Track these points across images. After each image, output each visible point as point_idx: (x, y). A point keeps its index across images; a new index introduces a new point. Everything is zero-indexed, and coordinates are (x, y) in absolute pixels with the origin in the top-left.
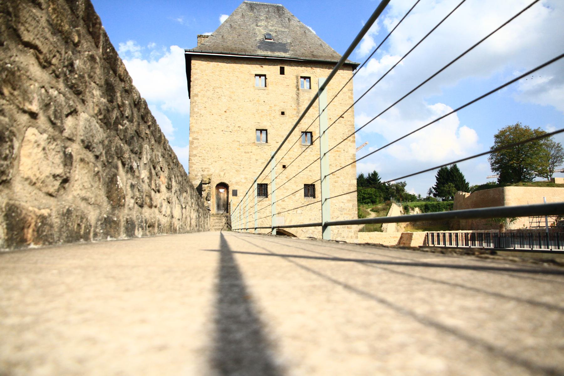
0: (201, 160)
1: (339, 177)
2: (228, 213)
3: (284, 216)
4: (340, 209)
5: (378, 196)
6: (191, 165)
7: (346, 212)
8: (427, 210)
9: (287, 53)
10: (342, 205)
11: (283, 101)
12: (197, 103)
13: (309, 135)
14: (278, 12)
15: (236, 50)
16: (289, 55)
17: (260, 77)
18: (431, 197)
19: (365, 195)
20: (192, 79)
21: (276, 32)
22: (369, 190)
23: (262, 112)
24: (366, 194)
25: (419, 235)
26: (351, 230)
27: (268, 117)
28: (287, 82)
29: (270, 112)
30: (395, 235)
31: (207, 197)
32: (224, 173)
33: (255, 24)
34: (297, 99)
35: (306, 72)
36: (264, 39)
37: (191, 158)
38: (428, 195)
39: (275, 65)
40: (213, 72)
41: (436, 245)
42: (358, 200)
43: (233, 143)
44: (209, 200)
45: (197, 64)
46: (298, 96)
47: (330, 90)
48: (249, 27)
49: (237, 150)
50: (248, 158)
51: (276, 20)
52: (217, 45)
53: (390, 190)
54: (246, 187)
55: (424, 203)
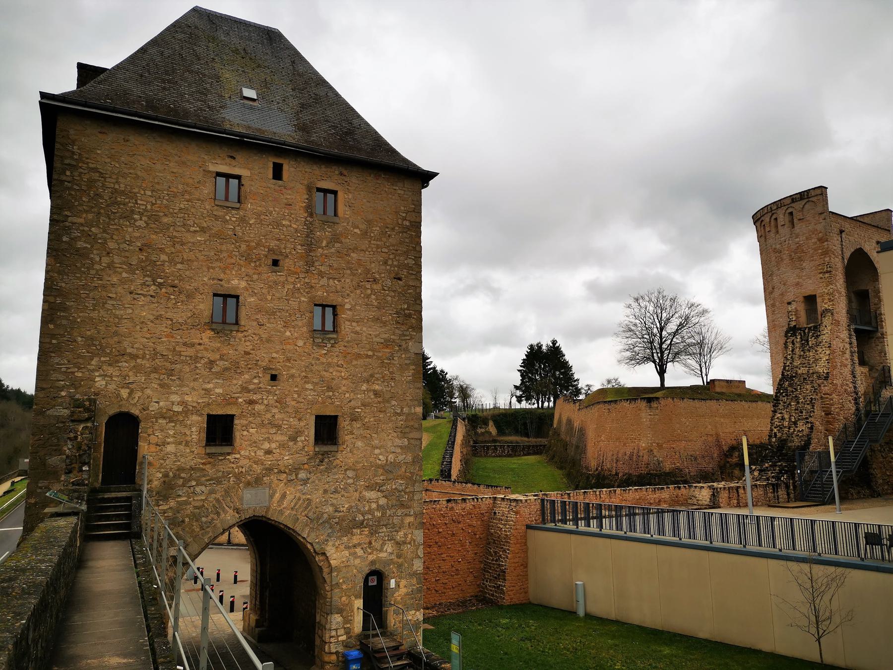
13: (329, 311)
14: (271, 44)
27: (243, 269)
43: (157, 322)
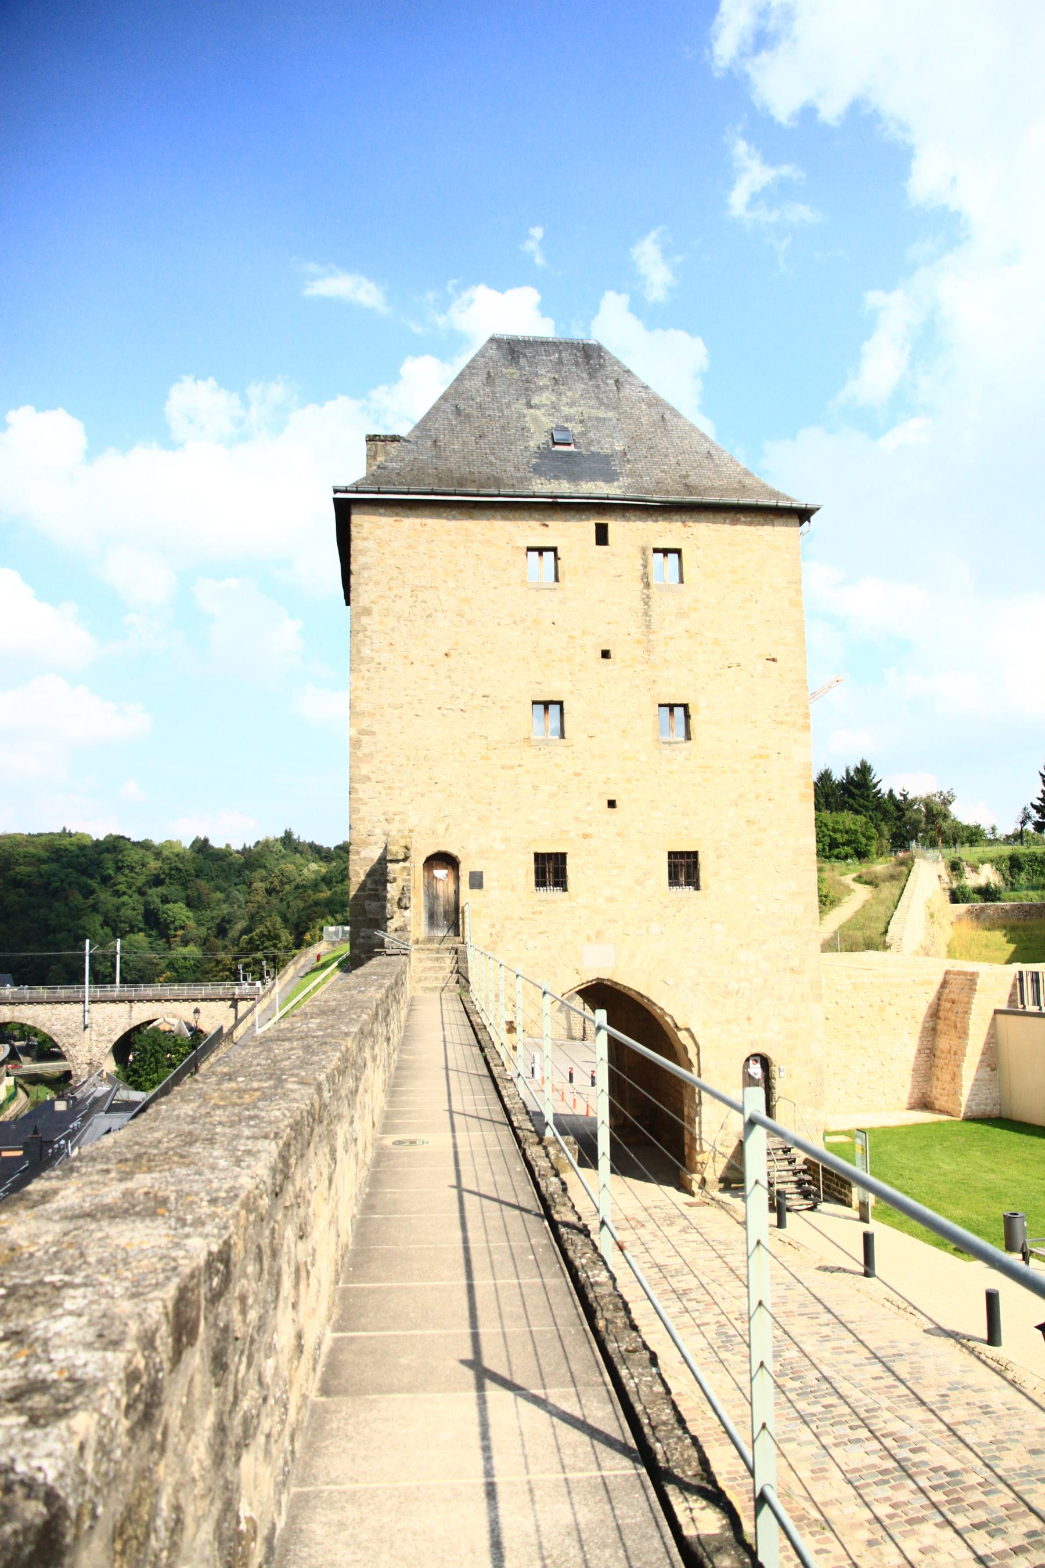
0: (383, 792)
1: (765, 830)
2: (458, 935)
5: (873, 838)
6: (355, 805)
8: (1016, 870)
9: (616, 483)
12: (368, 633)
13: (679, 712)
14: (588, 363)
15: (474, 481)
16: (620, 488)
19: (838, 836)
20: (353, 567)
21: (581, 422)
22: (848, 819)
23: (549, 651)
24: (841, 831)
31: (400, 899)
32: (444, 826)
33: (524, 401)
34: (646, 614)
36: (551, 443)
37: (356, 785)
39: (581, 520)
40: (410, 547)
44: (406, 908)
45: (366, 525)
46: (646, 603)
48: (506, 412)
51: (582, 386)
52: (422, 468)
53: (908, 814)
55: (1007, 850)
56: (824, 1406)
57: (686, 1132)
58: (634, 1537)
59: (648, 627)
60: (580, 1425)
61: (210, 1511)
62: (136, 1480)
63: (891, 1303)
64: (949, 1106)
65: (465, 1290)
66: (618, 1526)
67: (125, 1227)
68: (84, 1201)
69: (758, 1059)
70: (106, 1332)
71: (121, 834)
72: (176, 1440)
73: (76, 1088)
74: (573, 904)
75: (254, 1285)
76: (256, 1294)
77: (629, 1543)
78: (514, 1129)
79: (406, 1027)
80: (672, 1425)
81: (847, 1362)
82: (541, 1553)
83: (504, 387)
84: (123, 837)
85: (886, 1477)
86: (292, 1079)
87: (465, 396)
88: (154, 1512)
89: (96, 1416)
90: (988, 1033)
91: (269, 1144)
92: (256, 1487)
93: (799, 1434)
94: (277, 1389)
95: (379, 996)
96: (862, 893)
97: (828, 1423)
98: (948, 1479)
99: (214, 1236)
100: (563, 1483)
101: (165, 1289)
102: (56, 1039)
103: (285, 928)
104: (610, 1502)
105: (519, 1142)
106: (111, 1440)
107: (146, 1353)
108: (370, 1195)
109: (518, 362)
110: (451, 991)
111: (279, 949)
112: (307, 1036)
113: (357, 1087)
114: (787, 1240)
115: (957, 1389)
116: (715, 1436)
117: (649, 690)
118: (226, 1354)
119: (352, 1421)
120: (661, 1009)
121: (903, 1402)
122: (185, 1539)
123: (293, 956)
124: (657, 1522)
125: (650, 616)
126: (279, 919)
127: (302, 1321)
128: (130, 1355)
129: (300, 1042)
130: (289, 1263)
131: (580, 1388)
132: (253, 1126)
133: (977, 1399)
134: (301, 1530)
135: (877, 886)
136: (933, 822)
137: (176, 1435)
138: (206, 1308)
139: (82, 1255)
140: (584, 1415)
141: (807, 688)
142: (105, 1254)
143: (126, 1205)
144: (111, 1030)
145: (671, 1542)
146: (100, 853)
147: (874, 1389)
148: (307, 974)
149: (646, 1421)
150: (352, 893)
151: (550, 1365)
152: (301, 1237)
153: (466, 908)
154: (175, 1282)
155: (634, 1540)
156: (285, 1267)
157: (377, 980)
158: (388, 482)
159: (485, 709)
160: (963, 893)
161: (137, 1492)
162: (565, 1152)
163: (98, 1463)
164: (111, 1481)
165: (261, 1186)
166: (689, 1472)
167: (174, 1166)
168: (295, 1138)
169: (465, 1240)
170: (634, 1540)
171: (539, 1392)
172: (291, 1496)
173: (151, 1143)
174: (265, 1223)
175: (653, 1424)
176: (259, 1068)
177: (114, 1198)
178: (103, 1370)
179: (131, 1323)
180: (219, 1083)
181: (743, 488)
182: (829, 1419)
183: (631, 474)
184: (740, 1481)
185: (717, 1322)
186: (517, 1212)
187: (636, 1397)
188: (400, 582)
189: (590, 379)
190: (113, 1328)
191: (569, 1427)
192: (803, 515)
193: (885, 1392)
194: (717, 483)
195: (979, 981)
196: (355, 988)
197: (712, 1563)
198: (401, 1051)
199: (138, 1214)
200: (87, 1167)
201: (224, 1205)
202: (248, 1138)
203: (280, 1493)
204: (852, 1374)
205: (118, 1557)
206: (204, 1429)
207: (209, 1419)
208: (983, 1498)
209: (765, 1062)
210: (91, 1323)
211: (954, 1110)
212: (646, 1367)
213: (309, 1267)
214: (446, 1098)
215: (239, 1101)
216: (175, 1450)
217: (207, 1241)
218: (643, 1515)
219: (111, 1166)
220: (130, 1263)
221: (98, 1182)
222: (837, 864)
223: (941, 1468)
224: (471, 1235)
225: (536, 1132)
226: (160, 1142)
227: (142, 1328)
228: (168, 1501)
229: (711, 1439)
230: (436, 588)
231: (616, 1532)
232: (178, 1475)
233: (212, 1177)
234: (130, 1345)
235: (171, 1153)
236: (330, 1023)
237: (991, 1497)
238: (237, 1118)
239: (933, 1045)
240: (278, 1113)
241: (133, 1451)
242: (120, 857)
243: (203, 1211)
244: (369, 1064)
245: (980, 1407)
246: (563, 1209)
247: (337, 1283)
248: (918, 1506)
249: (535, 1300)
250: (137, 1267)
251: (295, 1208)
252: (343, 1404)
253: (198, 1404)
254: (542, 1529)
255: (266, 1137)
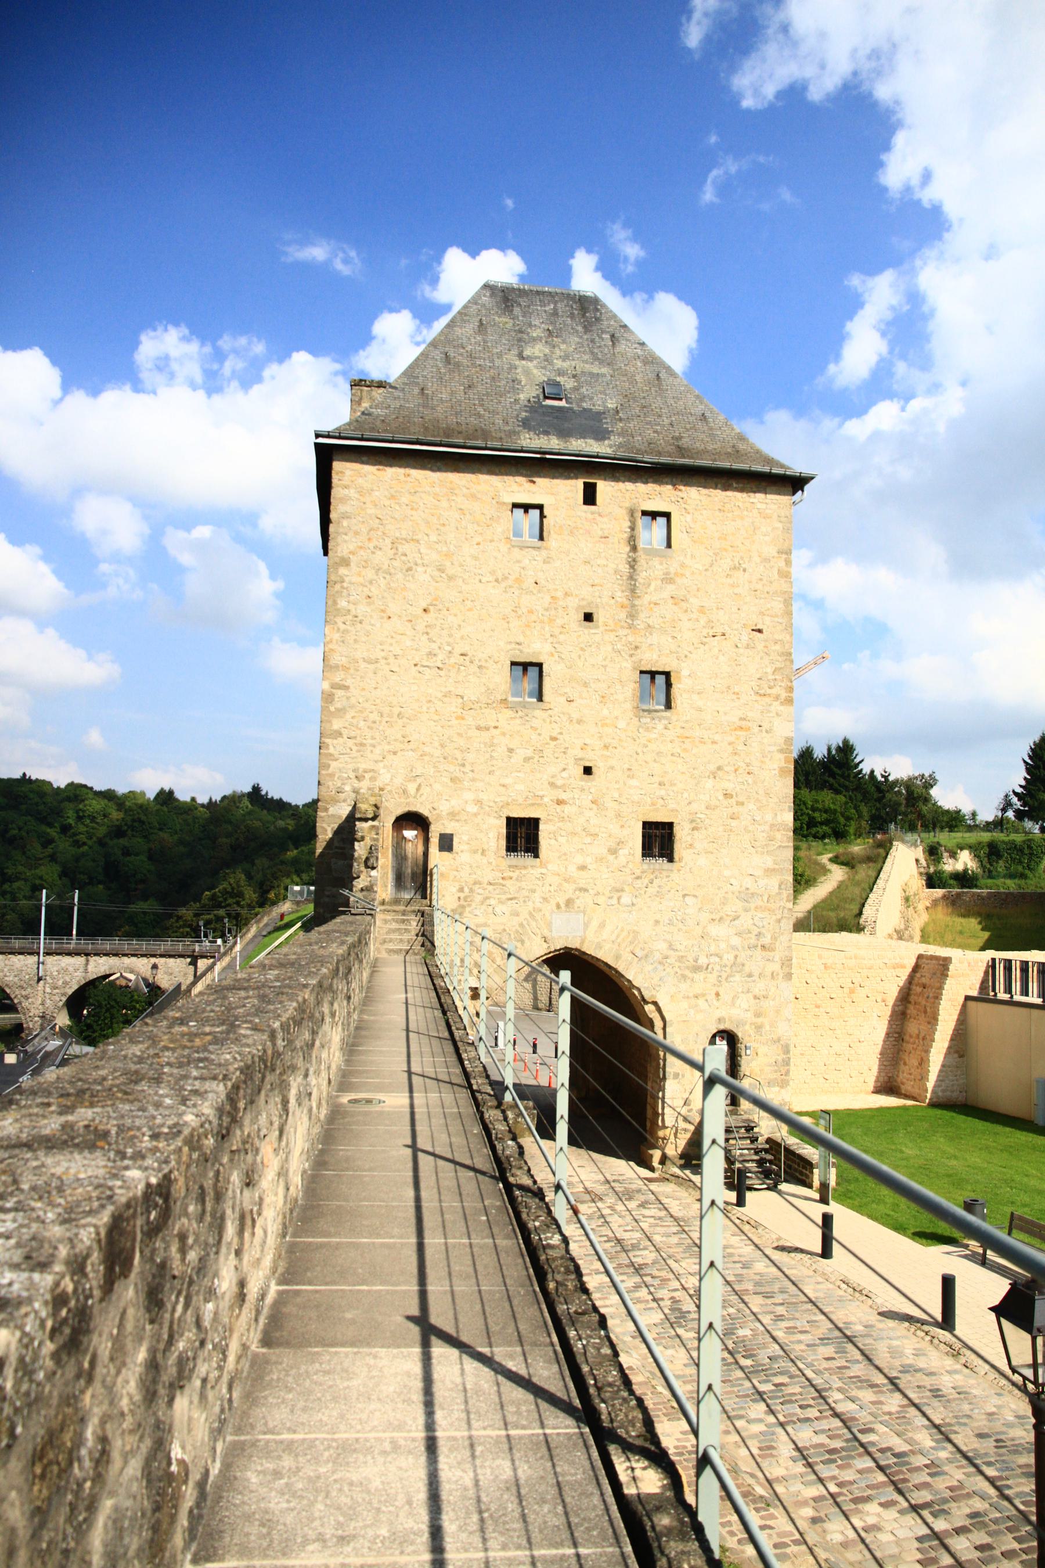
0: (355, 748)
1: (742, 804)
3: (584, 912)
4: (743, 895)
5: (852, 819)
6: (324, 761)
7: (760, 903)
8: (994, 858)
9: (606, 442)
10: (748, 882)
11: (591, 582)
12: (345, 585)
13: (660, 680)
14: (584, 316)
15: (460, 433)
16: (610, 446)
17: (526, 512)
18: (1008, 820)
19: (817, 815)
20: (333, 515)
21: (574, 376)
22: (827, 798)
23: (531, 612)
24: (820, 810)
25: (969, 964)
26: (771, 954)
27: (547, 628)
28: (604, 526)
29: (553, 612)
30: (898, 961)
31: (367, 859)
32: (415, 786)
33: (515, 352)
34: (631, 577)
35: (658, 498)
36: (541, 397)
37: (327, 741)
38: (1000, 814)
40: (393, 497)
41: (1018, 998)
42: (795, 831)
43: (446, 700)
44: (373, 868)
45: (348, 473)
46: (632, 567)
47: (726, 550)
48: (498, 362)
49: (454, 722)
50: (485, 744)
51: (577, 339)
53: (888, 796)
54: (478, 824)
55: (986, 837)
56: (775, 1385)
57: (648, 1107)
58: (574, 1494)
59: (633, 591)
60: (525, 1383)
61: (138, 1447)
62: (59, 1406)
63: (847, 1284)
64: (915, 1091)
65: (414, 1248)
66: (558, 1484)
67: (62, 1158)
68: (21, 1131)
69: (725, 1035)
70: (34, 1255)
71: (84, 782)
72: (105, 1371)
73: (28, 1042)
74: (544, 871)
75: (195, 1225)
76: (197, 1235)
77: (568, 1500)
78: (473, 1092)
79: (368, 988)
80: (618, 1387)
81: (800, 1342)
82: (479, 1506)
83: (495, 337)
84: (85, 786)
85: (833, 1457)
86: (245, 1026)
87: (455, 343)
88: (79, 1440)
89: (18, 1334)
90: (958, 1020)
91: (218, 1085)
92: (189, 1431)
93: (748, 1411)
94: (216, 1335)
95: (340, 952)
96: (837, 874)
97: (778, 1401)
98: (895, 1460)
99: (154, 1169)
100: (505, 1440)
101: (100, 1216)
102: (8, 991)
103: (249, 886)
104: (552, 1460)
105: (477, 1104)
106: (34, 1360)
107: (76, 1278)
108: (322, 1152)
109: (512, 311)
110: (416, 954)
111: (243, 907)
112: (263, 986)
113: (314, 1041)
114: (745, 1219)
115: (908, 1372)
116: (664, 1411)
117: (631, 656)
118: (162, 1291)
119: (293, 1372)
120: (629, 981)
121: (854, 1383)
122: (111, 1473)
123: (256, 915)
124: (597, 1480)
125: (636, 580)
126: (243, 876)
127: (245, 1270)
128: (58, 1277)
129: (256, 992)
130: (233, 1208)
131: (527, 1348)
132: (202, 1068)
133: (927, 1382)
134: (235, 1478)
135: (853, 867)
136: (913, 806)
137: (105, 1367)
138: (142, 1241)
139: (15, 1182)
140: (529, 1374)
141: (792, 662)
142: (39, 1182)
143: (65, 1137)
144: (66, 983)
145: (611, 1500)
146: (62, 801)
147: (826, 1369)
148: (270, 933)
149: (592, 1382)
150: (319, 851)
151: (497, 1324)
152: (248, 1185)
153: (435, 870)
154: (110, 1208)
155: (573, 1497)
156: (229, 1212)
157: (338, 937)
158: (372, 429)
159: (462, 668)
160: (940, 879)
161: (60, 1417)
162: (523, 1117)
163: (18, 1383)
164: (34, 1402)
165: (207, 1126)
166: (633, 1433)
167: (118, 1102)
168: (245, 1082)
169: (418, 1199)
170: (573, 1497)
171: (485, 1350)
172: (227, 1444)
173: (95, 1080)
174: (209, 1164)
175: (599, 1384)
176: (212, 1014)
177: (52, 1130)
178: (28, 1290)
179: (61, 1247)
180: (170, 1026)
181: (737, 453)
182: (780, 1397)
183: (622, 433)
184: (687, 1456)
185: (672, 1298)
186: (471, 1174)
187: (583, 1359)
188: (380, 533)
189: (585, 333)
190: (42, 1251)
191: (514, 1385)
192: (795, 483)
193: (836, 1373)
194: (710, 447)
195: (951, 967)
196: (317, 943)
197: (651, 1521)
198: (362, 1012)
199: (77, 1145)
200: (27, 1100)
201: (166, 1140)
202: (196, 1079)
203: (215, 1440)
204: (804, 1354)
205: (37, 1481)
206: (135, 1364)
207: (142, 1355)
208: (928, 1479)
209: (731, 1039)
210: (18, 1245)
211: (920, 1095)
212: (595, 1330)
213: (255, 1216)
214: (405, 1059)
215: (189, 1044)
216: (104, 1381)
217: (146, 1173)
218: (584, 1473)
219: (52, 1100)
220: (64, 1191)
221: (37, 1115)
222: (814, 844)
223: (889, 1449)
224: (424, 1194)
225: (495, 1096)
226: (104, 1079)
227: (72, 1252)
228: (94, 1433)
229: (660, 1413)
230: (418, 541)
231: (556, 1488)
232: (105, 1407)
233: (155, 1113)
234: (58, 1268)
235: (115, 1089)
236: (289, 975)
237: (936, 1479)
238: (186, 1060)
239: (902, 1028)
240: (228, 1057)
241: (58, 1376)
242: (81, 806)
243: (144, 1145)
244: (328, 1019)
245: (930, 1391)
246: (518, 1172)
247: (284, 1236)
248: (863, 1485)
249: (486, 1260)
250: (71, 1195)
251: (242, 1153)
252: (285, 1356)
253: (130, 1338)
254: (481, 1483)
255: (215, 1078)
